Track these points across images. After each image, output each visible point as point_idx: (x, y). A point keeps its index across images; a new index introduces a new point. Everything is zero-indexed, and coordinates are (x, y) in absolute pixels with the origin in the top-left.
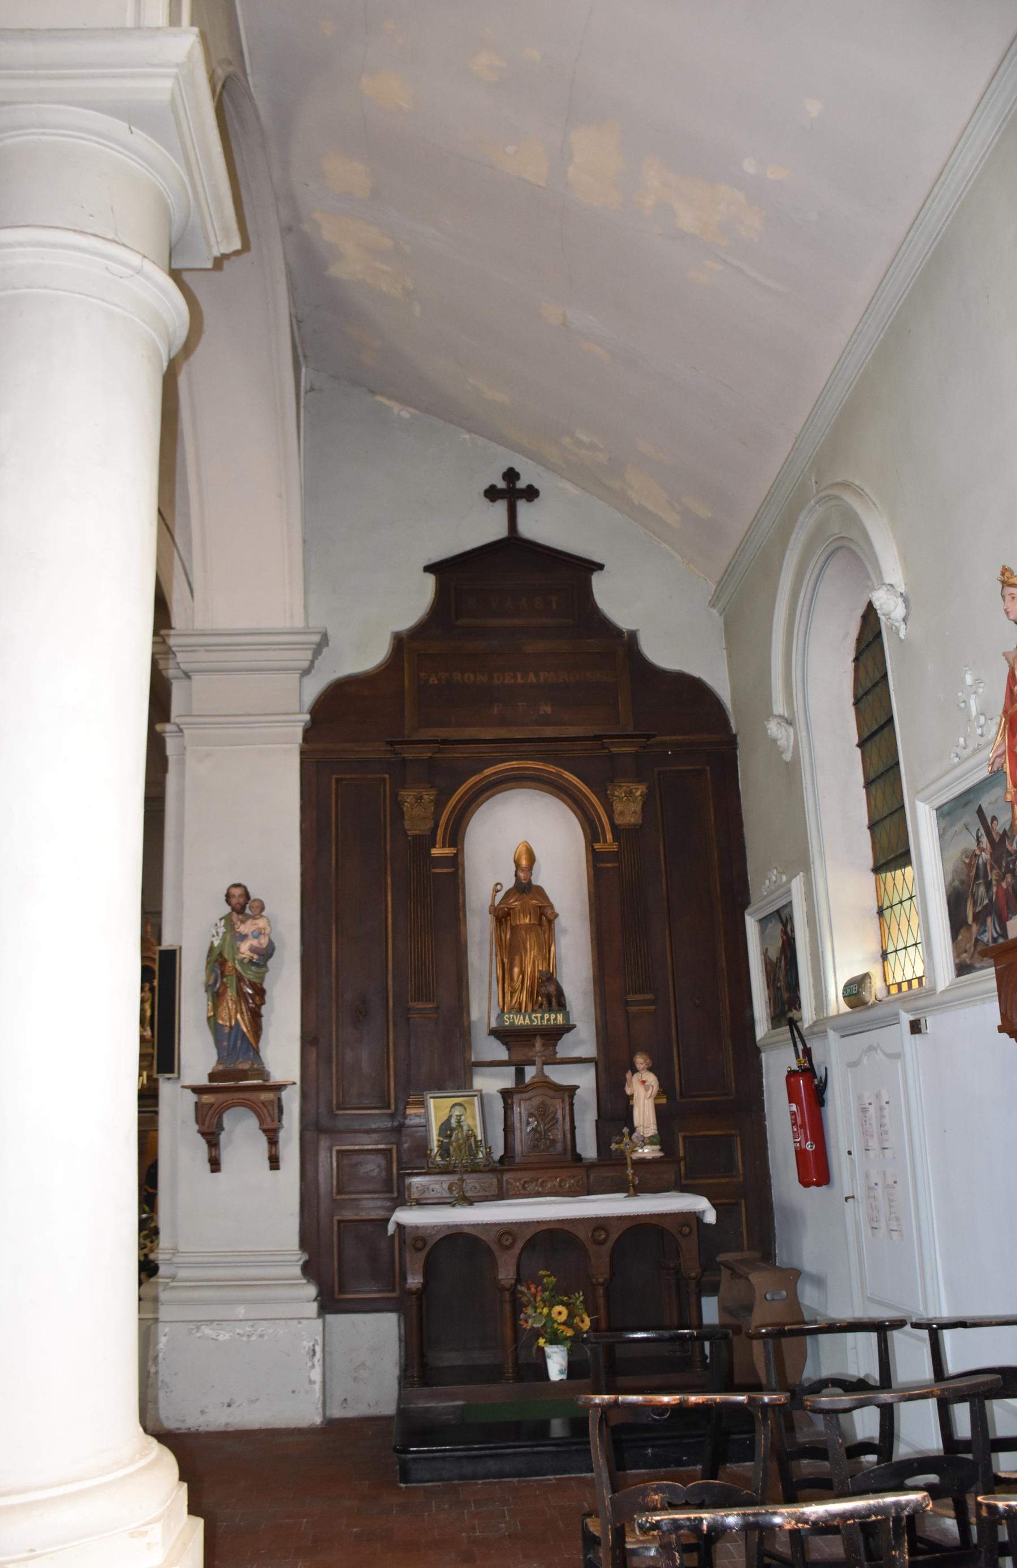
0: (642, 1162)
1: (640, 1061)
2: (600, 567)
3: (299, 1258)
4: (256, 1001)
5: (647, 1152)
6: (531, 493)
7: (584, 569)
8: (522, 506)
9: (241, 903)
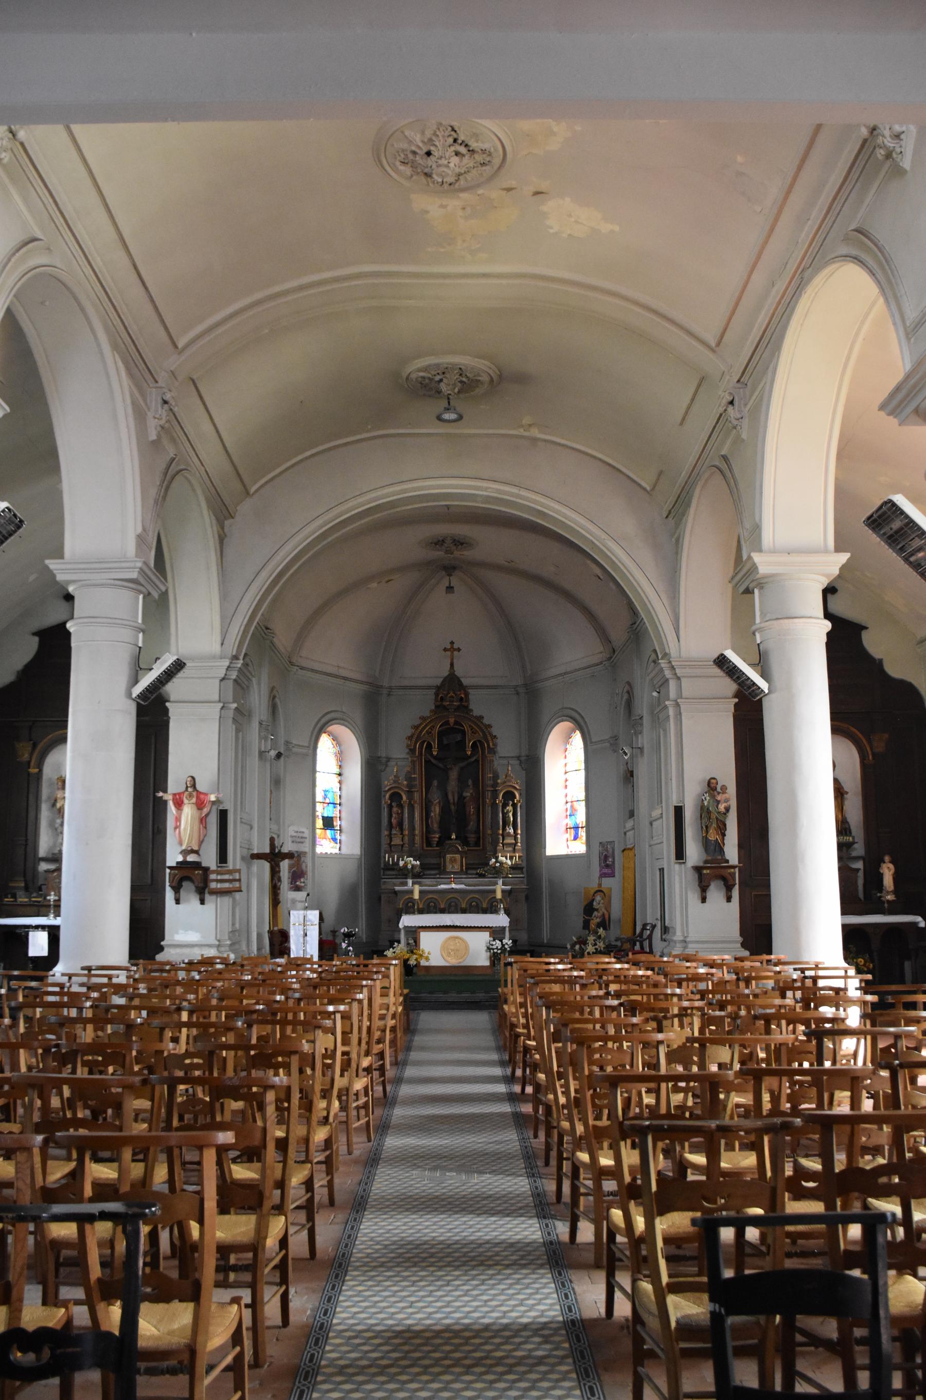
0: (888, 901)
1: (887, 858)
2: (866, 628)
3: (740, 939)
5: (890, 897)
9: (711, 786)
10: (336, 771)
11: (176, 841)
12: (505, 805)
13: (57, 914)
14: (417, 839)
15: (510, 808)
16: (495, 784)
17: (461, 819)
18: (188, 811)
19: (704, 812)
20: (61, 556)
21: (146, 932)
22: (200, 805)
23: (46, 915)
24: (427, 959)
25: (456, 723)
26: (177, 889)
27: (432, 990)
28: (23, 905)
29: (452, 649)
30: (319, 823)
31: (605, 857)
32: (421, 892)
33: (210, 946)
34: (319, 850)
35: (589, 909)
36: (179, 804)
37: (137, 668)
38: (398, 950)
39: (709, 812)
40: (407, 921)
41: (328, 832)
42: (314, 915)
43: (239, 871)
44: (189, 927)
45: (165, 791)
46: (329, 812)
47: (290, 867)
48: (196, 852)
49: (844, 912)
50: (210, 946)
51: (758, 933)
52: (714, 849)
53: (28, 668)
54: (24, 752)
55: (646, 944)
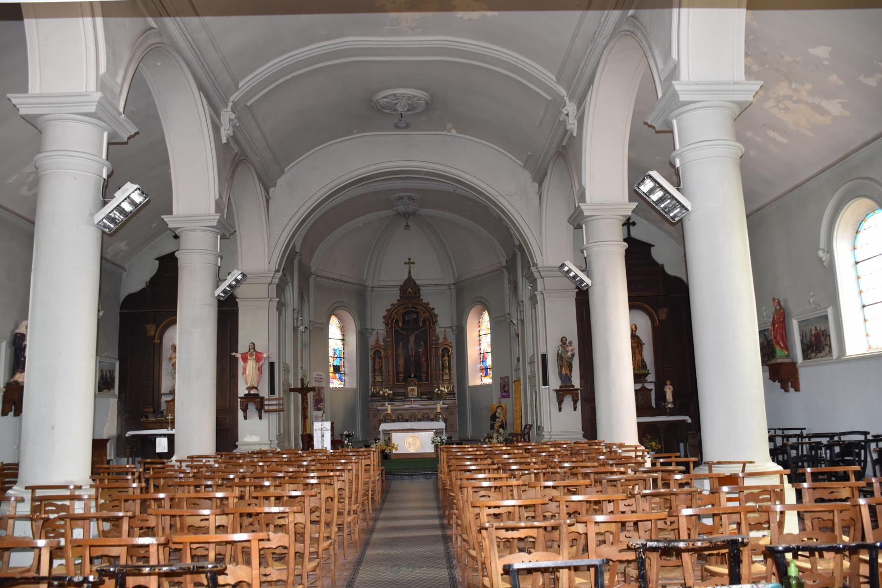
1: (668, 382)
2: (797, 389)
3: (582, 433)
4: (570, 366)
6: (634, 224)
7: (649, 246)
8: (631, 227)
9: (563, 341)
10: (338, 338)
11: (244, 382)
12: (443, 356)
13: (173, 428)
14: (391, 377)
15: (446, 358)
16: (437, 344)
17: (418, 363)
18: (251, 364)
19: (560, 357)
20: (171, 213)
21: (226, 435)
22: (258, 359)
23: (166, 428)
24: (396, 449)
25: (413, 307)
26: (245, 410)
27: (396, 467)
28: (152, 422)
29: (410, 263)
30: (331, 369)
31: (505, 387)
32: (392, 410)
33: (265, 444)
34: (331, 386)
35: (494, 417)
36: (245, 360)
37: (219, 281)
38: (378, 444)
39: (562, 357)
40: (384, 427)
41: (337, 375)
42: (328, 425)
43: (282, 399)
44: (252, 433)
45: (237, 352)
46: (337, 363)
47: (314, 396)
48: (256, 388)
49: (638, 416)
50: (265, 444)
51: (590, 427)
52: (566, 379)
53: (152, 279)
54: (151, 330)
55: (526, 437)
